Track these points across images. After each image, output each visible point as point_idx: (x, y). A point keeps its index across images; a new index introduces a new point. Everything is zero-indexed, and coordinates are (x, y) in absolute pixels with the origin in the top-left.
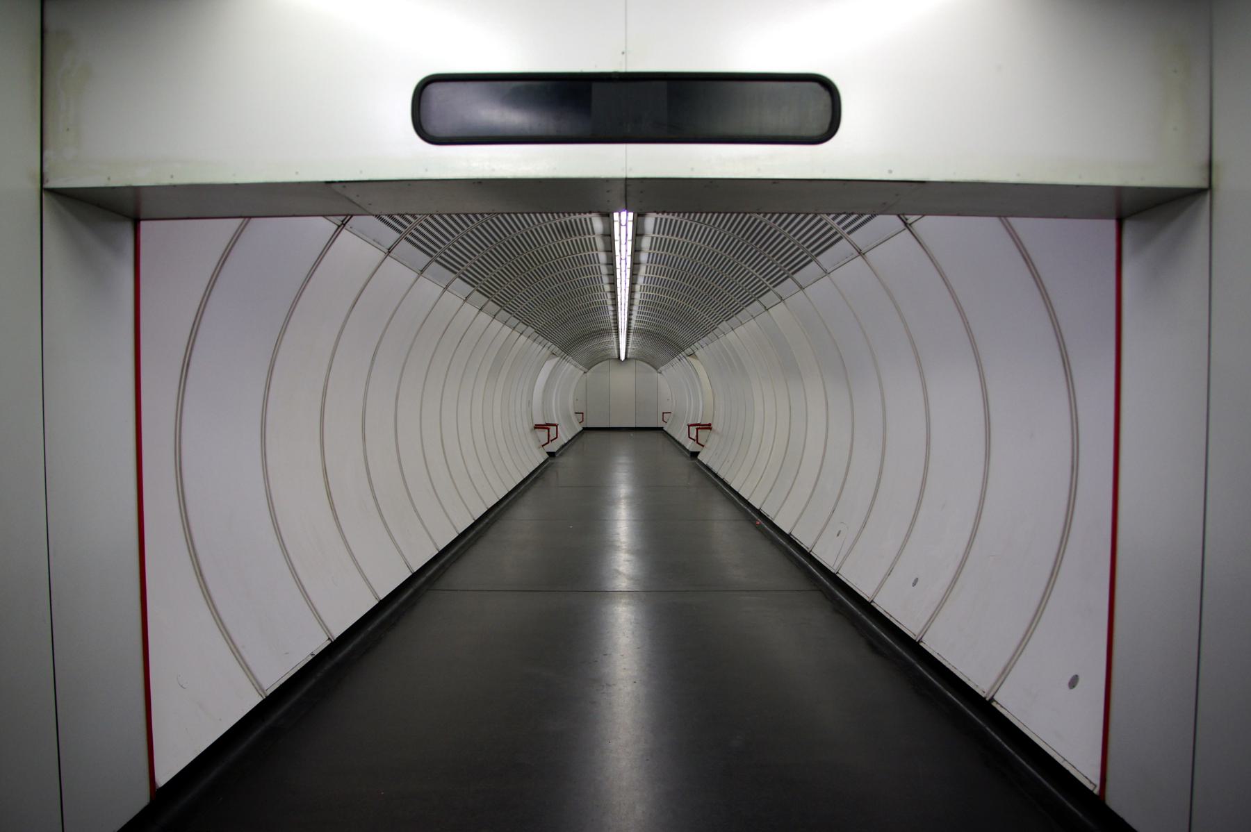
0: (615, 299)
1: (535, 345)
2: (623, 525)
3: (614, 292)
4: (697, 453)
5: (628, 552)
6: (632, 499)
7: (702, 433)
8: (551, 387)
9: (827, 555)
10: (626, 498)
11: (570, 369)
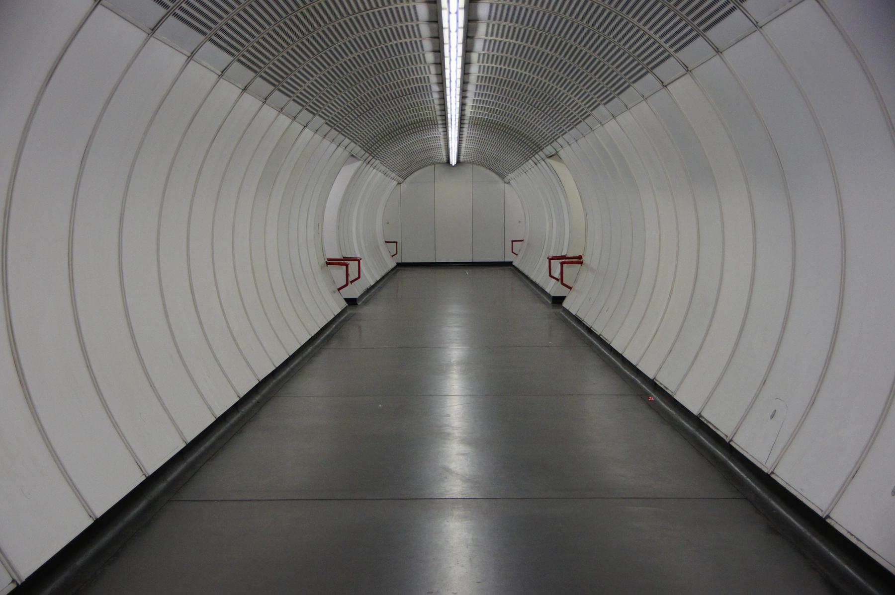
0: (441, 74)
1: (326, 142)
2: (455, 403)
3: (440, 64)
4: (563, 298)
5: (464, 441)
6: (468, 365)
7: (570, 271)
8: (348, 204)
9: (756, 447)
10: (460, 363)
11: (377, 178)
